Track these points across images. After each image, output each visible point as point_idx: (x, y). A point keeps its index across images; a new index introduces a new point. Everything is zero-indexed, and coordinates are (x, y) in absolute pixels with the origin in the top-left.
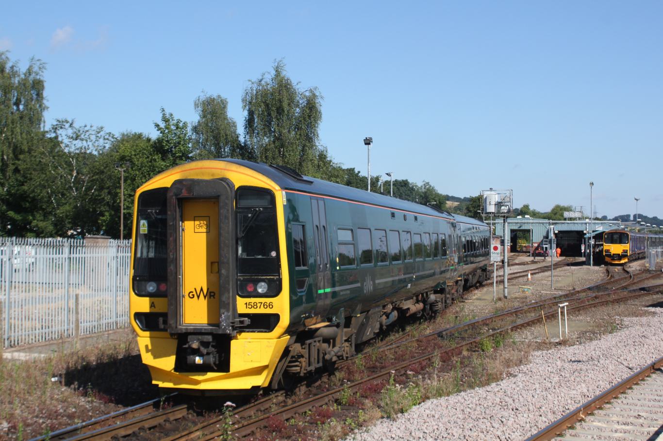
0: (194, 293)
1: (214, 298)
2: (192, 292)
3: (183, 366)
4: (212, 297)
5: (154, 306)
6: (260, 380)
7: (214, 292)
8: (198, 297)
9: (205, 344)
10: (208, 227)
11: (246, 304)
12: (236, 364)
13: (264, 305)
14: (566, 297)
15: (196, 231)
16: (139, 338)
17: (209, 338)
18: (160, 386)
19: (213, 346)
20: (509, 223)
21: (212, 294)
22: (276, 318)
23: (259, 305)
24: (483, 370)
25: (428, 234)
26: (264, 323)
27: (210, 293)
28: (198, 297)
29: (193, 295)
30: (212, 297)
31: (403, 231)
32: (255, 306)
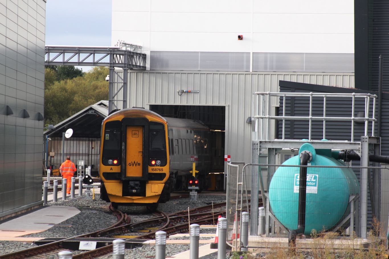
0: (131, 164)
2: (130, 163)
3: (126, 192)
4: (139, 165)
5: (112, 169)
6: (155, 201)
7: (140, 163)
8: (133, 165)
9: (137, 185)
10: (144, 134)
11: (152, 169)
12: (148, 193)
13: (159, 170)
14: (179, 198)
15: (133, 136)
16: (104, 183)
17: (137, 183)
18: (194, 186)
19: (139, 186)
20: (367, 98)
21: (139, 164)
22: (165, 175)
23: (157, 170)
24: (54, 229)
25: (188, 140)
26: (160, 177)
27: (138, 163)
28: (133, 165)
29: (131, 164)
30: (139, 165)
31: (183, 139)
32: (156, 170)
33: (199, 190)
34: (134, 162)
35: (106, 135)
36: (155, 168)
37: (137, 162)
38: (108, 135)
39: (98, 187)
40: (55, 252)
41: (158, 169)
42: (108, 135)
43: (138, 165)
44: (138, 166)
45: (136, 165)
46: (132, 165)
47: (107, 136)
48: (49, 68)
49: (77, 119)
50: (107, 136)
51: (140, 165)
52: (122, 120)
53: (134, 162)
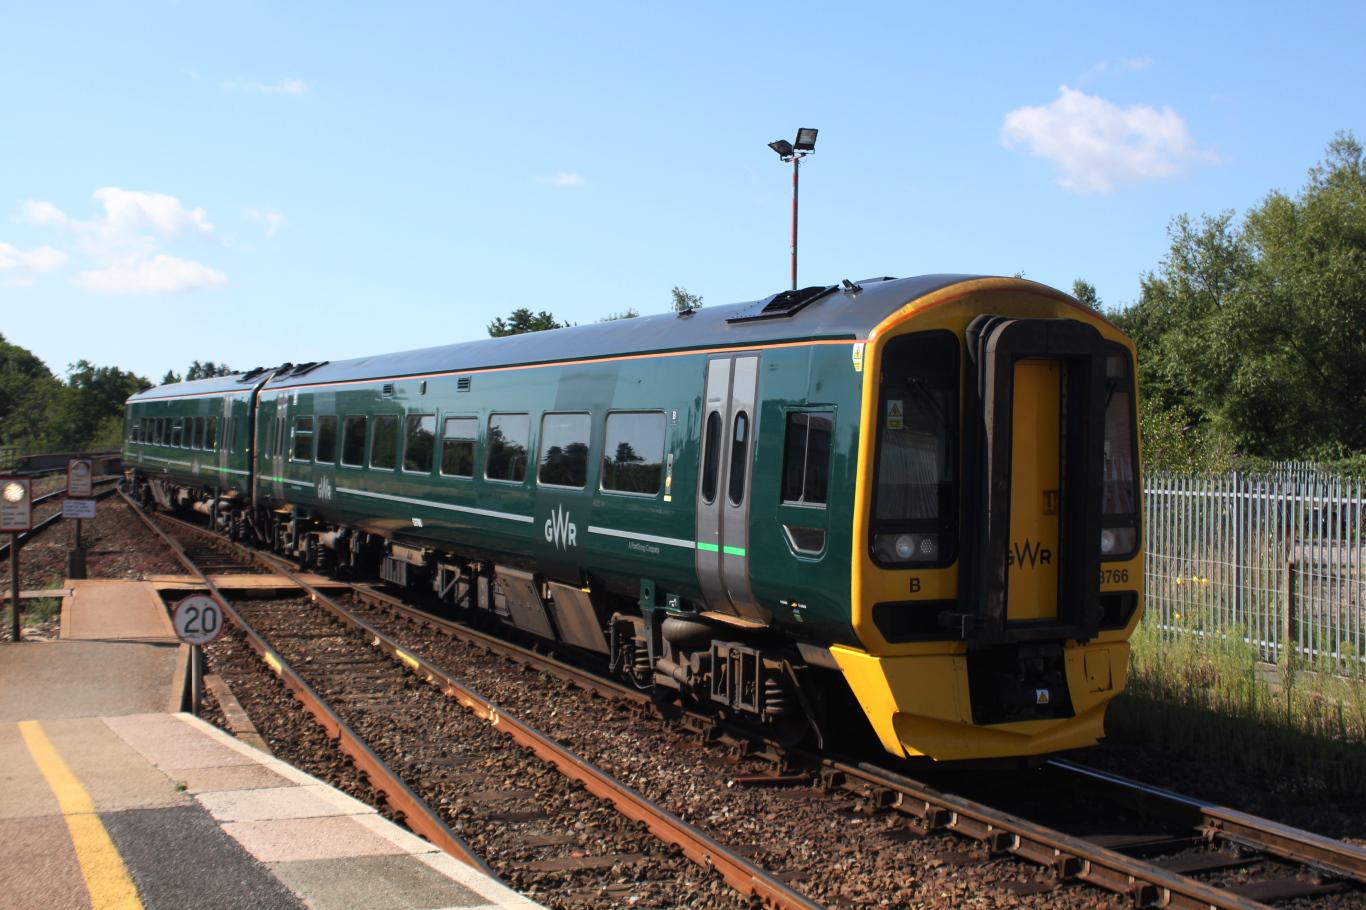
1: (1049, 562)
4: (1315, 167)
8: (1021, 561)
21: (1046, 555)
27: (1043, 551)
28: (1021, 561)
33: (404, 588)
34: (1027, 546)
35: (891, 404)
36: (1121, 570)
37: (1039, 544)
38: (900, 404)
39: (740, 438)
40: (941, 806)
41: (1110, 572)
42: (900, 404)
43: (1042, 558)
44: (1042, 562)
45: (1033, 561)
46: (1016, 559)
47: (895, 409)
48: (1261, 725)
49: (1178, 802)
50: (895, 409)
51: (1047, 559)
52: (1106, 733)
53: (1027, 546)
